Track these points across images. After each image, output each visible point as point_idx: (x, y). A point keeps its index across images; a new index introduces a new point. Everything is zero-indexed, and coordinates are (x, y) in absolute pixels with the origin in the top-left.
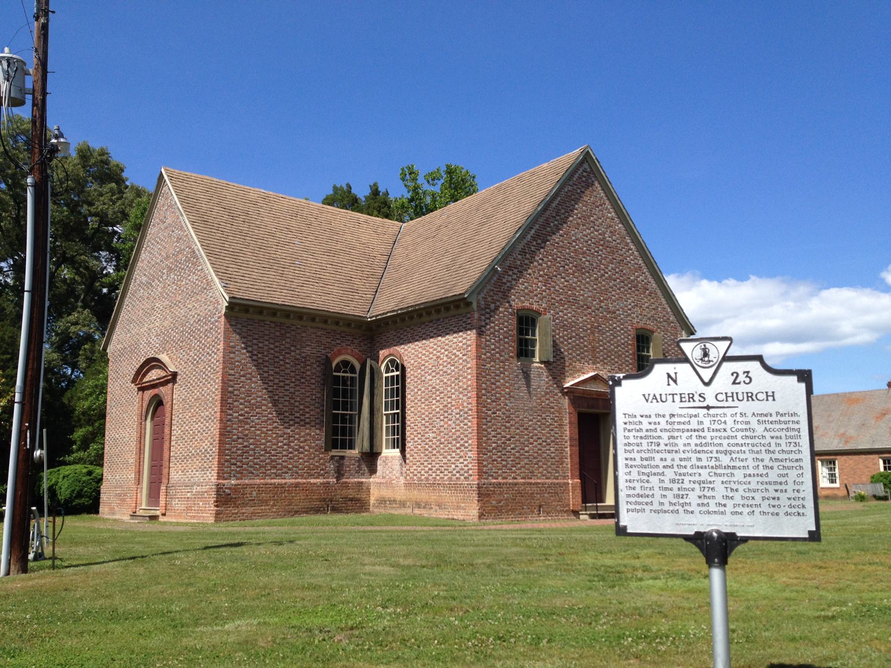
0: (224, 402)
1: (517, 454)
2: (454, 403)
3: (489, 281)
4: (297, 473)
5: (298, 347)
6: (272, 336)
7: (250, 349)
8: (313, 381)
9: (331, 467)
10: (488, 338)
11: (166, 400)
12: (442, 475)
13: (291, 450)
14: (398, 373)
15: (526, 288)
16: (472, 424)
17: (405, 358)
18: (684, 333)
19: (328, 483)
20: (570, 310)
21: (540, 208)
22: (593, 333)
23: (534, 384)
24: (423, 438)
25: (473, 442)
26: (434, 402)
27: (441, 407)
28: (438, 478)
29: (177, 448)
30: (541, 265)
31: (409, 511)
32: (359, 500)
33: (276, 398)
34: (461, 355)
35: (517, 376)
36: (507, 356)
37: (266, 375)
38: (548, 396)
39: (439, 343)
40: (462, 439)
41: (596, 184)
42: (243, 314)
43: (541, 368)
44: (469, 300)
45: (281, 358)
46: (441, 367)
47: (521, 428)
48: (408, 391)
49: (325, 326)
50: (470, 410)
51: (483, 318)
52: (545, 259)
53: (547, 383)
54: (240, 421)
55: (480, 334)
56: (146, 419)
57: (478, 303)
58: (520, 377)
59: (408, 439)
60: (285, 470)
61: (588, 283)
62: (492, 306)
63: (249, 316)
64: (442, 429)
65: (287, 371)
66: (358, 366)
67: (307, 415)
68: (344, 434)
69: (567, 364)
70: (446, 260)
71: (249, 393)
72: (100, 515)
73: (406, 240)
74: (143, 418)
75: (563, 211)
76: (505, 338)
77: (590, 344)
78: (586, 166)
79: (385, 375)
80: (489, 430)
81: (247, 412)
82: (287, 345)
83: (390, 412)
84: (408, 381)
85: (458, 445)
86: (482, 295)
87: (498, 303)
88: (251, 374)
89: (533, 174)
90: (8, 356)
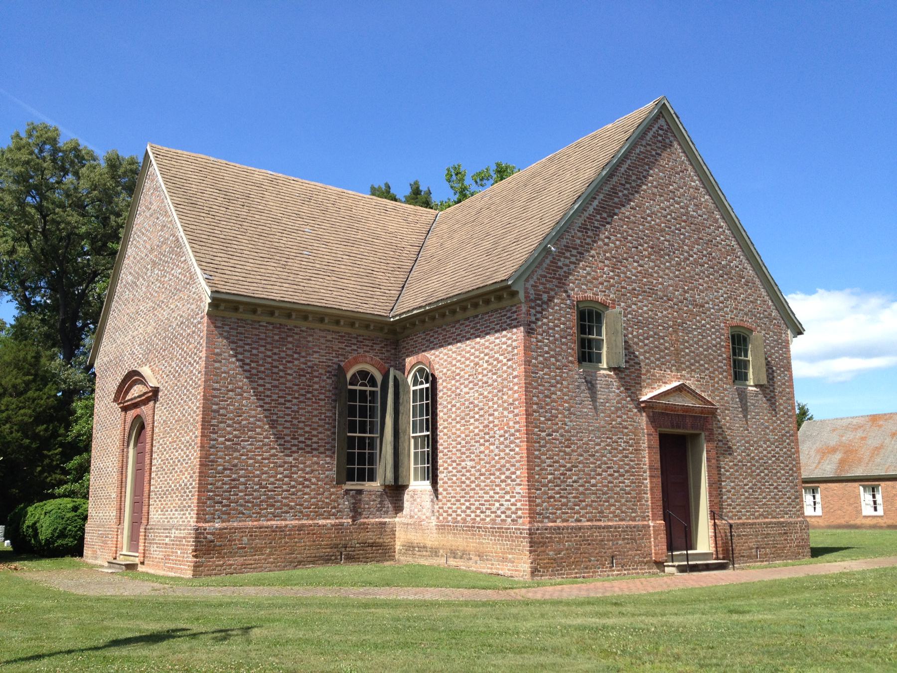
0: (206, 423)
1: (581, 489)
2: (496, 422)
3: (540, 264)
4: (301, 512)
5: (303, 354)
6: (269, 340)
7: (240, 357)
8: (322, 397)
9: (345, 504)
10: (540, 337)
11: (148, 421)
12: (482, 516)
13: (293, 483)
14: (428, 385)
15: (589, 274)
16: (520, 449)
17: (436, 366)
18: (789, 332)
19: (342, 524)
20: (645, 302)
21: (604, 173)
22: (675, 331)
23: (601, 397)
24: (459, 468)
26: (472, 421)
27: (481, 427)
28: (478, 519)
29: (157, 482)
30: (607, 244)
31: (443, 561)
32: (380, 545)
33: (275, 417)
34: (505, 361)
35: (579, 387)
36: (564, 361)
38: (619, 413)
39: (477, 346)
40: (508, 469)
41: (676, 145)
42: (232, 313)
43: (609, 376)
44: (514, 288)
46: (480, 377)
48: (440, 408)
49: (336, 328)
50: (518, 431)
51: (533, 311)
52: (613, 238)
53: (618, 395)
55: (529, 332)
57: (526, 292)
58: (583, 388)
59: (441, 469)
60: (285, 509)
61: (668, 268)
62: (545, 297)
63: (239, 316)
64: (482, 456)
65: (289, 384)
66: (379, 378)
67: (315, 439)
68: (362, 460)
69: (644, 371)
70: (487, 244)
72: (84, 558)
73: (441, 229)
75: (634, 177)
76: (562, 337)
77: (672, 345)
78: (661, 122)
79: (412, 388)
80: (544, 457)
81: (236, 436)
84: (440, 394)
85: (503, 477)
86: (532, 282)
87: (552, 293)
88: (241, 388)
89: (595, 137)
90: (31, 377)
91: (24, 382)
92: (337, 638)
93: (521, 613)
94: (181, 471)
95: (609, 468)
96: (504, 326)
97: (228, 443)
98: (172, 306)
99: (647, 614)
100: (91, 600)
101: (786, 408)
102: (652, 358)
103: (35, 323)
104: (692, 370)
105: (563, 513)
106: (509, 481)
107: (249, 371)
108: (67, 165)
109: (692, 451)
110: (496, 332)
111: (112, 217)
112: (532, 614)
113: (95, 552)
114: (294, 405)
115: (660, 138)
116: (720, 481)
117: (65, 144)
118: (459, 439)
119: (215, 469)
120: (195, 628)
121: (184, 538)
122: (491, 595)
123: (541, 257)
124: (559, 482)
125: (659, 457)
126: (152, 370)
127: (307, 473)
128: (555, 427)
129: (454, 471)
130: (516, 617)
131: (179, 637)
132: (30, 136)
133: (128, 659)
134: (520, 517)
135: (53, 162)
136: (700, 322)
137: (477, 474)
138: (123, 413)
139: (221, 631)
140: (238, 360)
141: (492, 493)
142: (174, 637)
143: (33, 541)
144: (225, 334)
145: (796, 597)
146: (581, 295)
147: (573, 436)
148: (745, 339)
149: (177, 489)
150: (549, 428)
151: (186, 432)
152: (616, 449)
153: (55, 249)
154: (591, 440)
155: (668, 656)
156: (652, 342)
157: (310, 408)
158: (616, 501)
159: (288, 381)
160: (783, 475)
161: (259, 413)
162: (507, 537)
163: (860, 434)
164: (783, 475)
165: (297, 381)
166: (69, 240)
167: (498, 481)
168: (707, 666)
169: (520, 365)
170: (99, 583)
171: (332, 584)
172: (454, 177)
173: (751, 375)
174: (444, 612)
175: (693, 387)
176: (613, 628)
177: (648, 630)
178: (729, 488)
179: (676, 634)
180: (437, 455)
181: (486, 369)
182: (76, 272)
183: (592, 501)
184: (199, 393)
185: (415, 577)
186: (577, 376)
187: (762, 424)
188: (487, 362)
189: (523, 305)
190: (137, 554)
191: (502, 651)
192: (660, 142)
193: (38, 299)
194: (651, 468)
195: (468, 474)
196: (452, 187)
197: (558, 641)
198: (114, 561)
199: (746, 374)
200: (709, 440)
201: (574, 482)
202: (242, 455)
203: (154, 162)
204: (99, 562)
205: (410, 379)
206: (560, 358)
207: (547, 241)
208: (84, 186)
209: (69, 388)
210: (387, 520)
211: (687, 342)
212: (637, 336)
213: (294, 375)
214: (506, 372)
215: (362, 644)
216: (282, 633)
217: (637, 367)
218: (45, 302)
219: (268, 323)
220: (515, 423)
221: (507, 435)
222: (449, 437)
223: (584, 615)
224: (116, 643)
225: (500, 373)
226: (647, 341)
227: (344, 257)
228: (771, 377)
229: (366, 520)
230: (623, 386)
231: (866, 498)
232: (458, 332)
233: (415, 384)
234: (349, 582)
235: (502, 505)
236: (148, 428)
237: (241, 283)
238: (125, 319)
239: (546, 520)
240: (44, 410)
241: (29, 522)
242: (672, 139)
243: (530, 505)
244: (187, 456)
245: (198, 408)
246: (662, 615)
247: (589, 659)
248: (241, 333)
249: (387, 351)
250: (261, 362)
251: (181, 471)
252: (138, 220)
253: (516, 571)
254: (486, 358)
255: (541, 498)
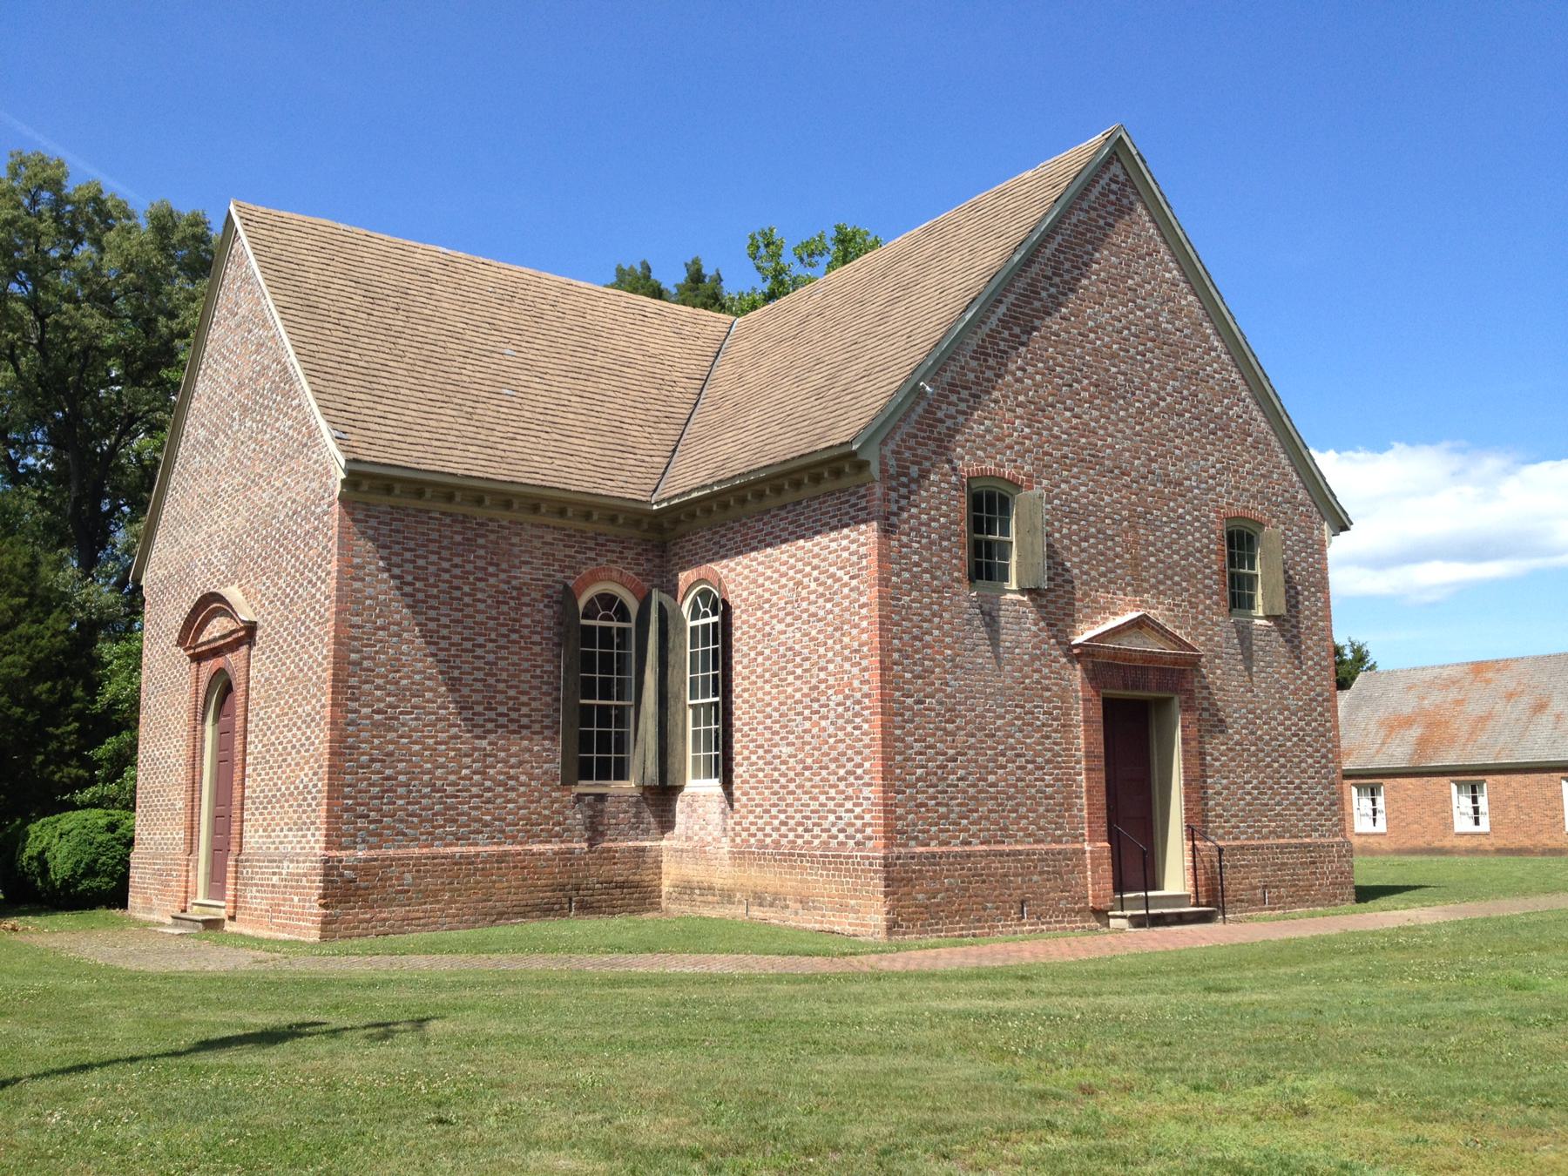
1: (971, 791)
2: (831, 681)
3: (907, 415)
4: (502, 832)
5: (504, 566)
6: (445, 542)
7: (396, 571)
8: (536, 638)
9: (577, 817)
10: (905, 539)
12: (807, 836)
13: (488, 784)
14: (716, 619)
15: (988, 431)
16: (871, 726)
17: (731, 587)
18: (1326, 526)
19: (571, 852)
20: (1083, 477)
21: (1017, 258)
22: (1133, 527)
23: (1007, 639)
24: (769, 757)
25: (872, 765)
26: (791, 678)
27: (806, 690)
29: (256, 782)
30: (1018, 380)
32: (637, 886)
33: (456, 673)
34: (846, 578)
36: (946, 578)
37: (432, 625)
38: (1037, 664)
39: (800, 554)
40: (850, 760)
41: (1139, 208)
42: (373, 492)
44: (862, 457)
45: (466, 589)
46: (804, 605)
47: (980, 735)
48: (736, 657)
50: (867, 696)
51: (893, 495)
52: (1030, 369)
54: (375, 725)
55: (887, 531)
56: (204, 720)
57: (883, 463)
59: (738, 759)
60: (475, 826)
61: (1122, 420)
62: (914, 471)
63: (392, 500)
64: (807, 738)
65: (479, 618)
66: (633, 606)
67: (525, 710)
68: (604, 745)
69: (1079, 594)
70: (817, 379)
71: (396, 665)
73: (739, 348)
74: (199, 718)
75: (1067, 265)
76: (942, 538)
78: (1115, 169)
79: (690, 624)
80: (909, 739)
82: (480, 563)
83: (700, 701)
84: (737, 634)
85: (842, 772)
86: (892, 446)
87: (927, 464)
88: (399, 624)
89: (1002, 193)
90: (23, 600)
91: (11, 607)
92: (569, 1034)
93: (868, 993)
94: (297, 764)
95: (1018, 755)
96: (846, 519)
97: (376, 717)
98: (277, 484)
99: (1071, 994)
100: (154, 980)
101: (1317, 654)
102: (1093, 573)
103: (27, 505)
104: (1160, 593)
105: (941, 831)
106: (851, 779)
107: (412, 595)
108: (81, 228)
109: (1158, 723)
110: (832, 529)
111: (162, 320)
112: (885, 994)
113: (148, 900)
114: (488, 652)
115: (1112, 197)
116: (1204, 777)
117: (76, 191)
118: (769, 710)
119: (357, 761)
120: (334, 1021)
121: (305, 875)
122: (819, 964)
123: (910, 402)
124: (934, 779)
125: (1101, 737)
126: (245, 593)
127: (512, 767)
128: (928, 690)
129: (761, 762)
130: (858, 999)
131: (310, 1035)
132: (15, 175)
133: (232, 1069)
134: (870, 838)
135: (55, 221)
136: (1174, 511)
137: (799, 768)
138: (194, 665)
139: (378, 1025)
140: (393, 577)
141: (822, 798)
142: (301, 1035)
143: (39, 883)
144: (370, 532)
145: (1320, 965)
146: (975, 467)
147: (959, 703)
148: (1250, 539)
149: (291, 794)
150: (919, 691)
151: (305, 698)
152: (1031, 725)
153: (61, 375)
154: (988, 711)
155: (1097, 1057)
156: (1094, 546)
157: (515, 658)
158: (1029, 811)
159: (478, 612)
160: (1311, 766)
161: (429, 665)
162: (847, 870)
163: (1453, 694)
164: (1311, 766)
165: (494, 612)
166: (86, 358)
167: (833, 779)
168: (1157, 1071)
169: (871, 586)
170: (161, 952)
171: (557, 950)
172: (763, 251)
173: (1259, 600)
174: (741, 992)
175: (1161, 621)
176: (1013, 1015)
177: (1070, 1018)
178: (1218, 787)
179: (1114, 1023)
180: (731, 736)
181: (814, 592)
182: (97, 414)
183: (990, 811)
184: (327, 633)
185: (695, 937)
186: (966, 604)
187: (1277, 681)
188: (816, 580)
189: (877, 485)
190: (222, 904)
191: (834, 1050)
192: (1113, 204)
193: (31, 461)
194: (1088, 755)
195: (783, 767)
196: (758, 268)
197: (924, 1035)
198: (183, 915)
199: (1251, 598)
200: (1187, 708)
201: (959, 779)
202: (401, 737)
203: (241, 232)
204: (155, 917)
205: (686, 609)
206: (939, 573)
207: (918, 375)
208: (111, 264)
209: (90, 619)
210: (647, 844)
211: (1154, 545)
212: (1068, 536)
213: (489, 601)
214: (847, 597)
215: (610, 1042)
216: (478, 1027)
217: (1068, 587)
218: (43, 466)
219: (443, 513)
220: (862, 683)
221: (848, 703)
222: (752, 707)
223: (970, 995)
224: (207, 1045)
225: (837, 598)
226: (1085, 545)
227: (573, 398)
228: (1293, 602)
229: (611, 845)
230: (1044, 619)
231: (1461, 803)
232: (768, 529)
233: (694, 617)
234: (584, 947)
235: (840, 818)
236: (239, 692)
237: (396, 444)
238: (195, 504)
239: (913, 843)
240: (48, 657)
241: (32, 850)
242: (1133, 198)
243: (886, 819)
244: (308, 738)
245: (325, 658)
246: (1096, 995)
247: (972, 1061)
248: (398, 531)
249: (648, 560)
250: (432, 580)
251: (297, 764)
252: (215, 333)
253: (863, 925)
254: (815, 573)
255: (904, 806)
